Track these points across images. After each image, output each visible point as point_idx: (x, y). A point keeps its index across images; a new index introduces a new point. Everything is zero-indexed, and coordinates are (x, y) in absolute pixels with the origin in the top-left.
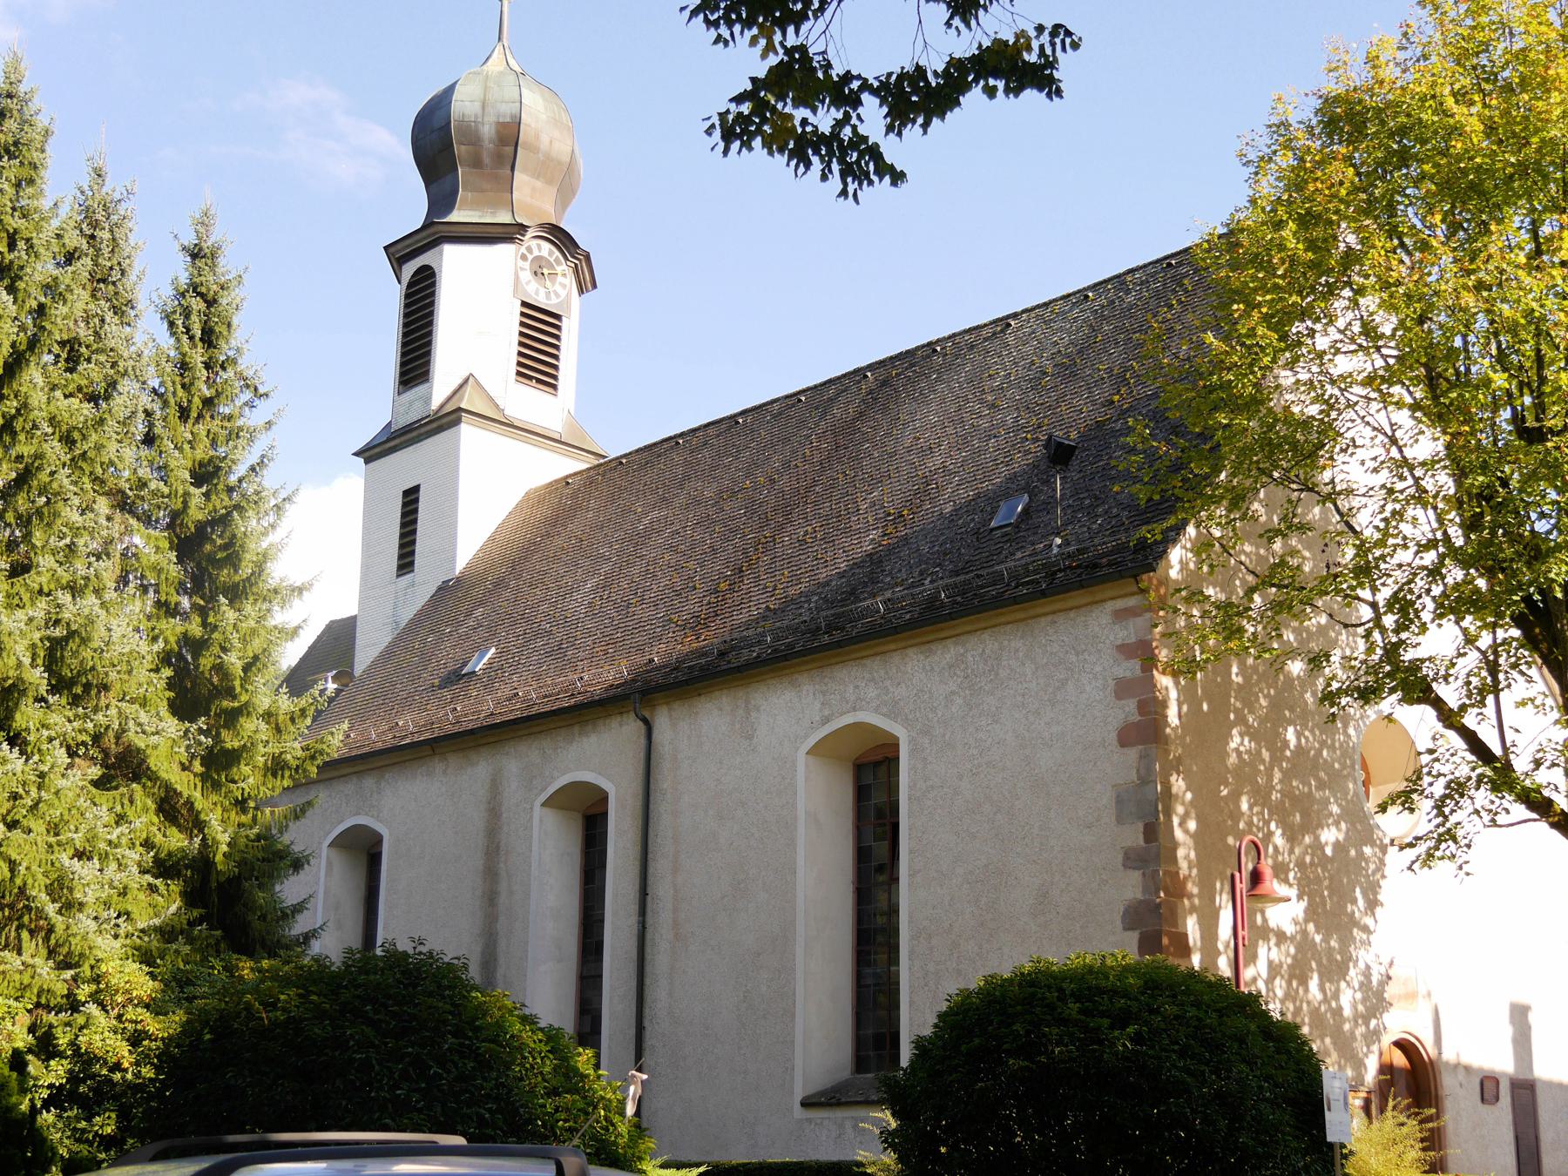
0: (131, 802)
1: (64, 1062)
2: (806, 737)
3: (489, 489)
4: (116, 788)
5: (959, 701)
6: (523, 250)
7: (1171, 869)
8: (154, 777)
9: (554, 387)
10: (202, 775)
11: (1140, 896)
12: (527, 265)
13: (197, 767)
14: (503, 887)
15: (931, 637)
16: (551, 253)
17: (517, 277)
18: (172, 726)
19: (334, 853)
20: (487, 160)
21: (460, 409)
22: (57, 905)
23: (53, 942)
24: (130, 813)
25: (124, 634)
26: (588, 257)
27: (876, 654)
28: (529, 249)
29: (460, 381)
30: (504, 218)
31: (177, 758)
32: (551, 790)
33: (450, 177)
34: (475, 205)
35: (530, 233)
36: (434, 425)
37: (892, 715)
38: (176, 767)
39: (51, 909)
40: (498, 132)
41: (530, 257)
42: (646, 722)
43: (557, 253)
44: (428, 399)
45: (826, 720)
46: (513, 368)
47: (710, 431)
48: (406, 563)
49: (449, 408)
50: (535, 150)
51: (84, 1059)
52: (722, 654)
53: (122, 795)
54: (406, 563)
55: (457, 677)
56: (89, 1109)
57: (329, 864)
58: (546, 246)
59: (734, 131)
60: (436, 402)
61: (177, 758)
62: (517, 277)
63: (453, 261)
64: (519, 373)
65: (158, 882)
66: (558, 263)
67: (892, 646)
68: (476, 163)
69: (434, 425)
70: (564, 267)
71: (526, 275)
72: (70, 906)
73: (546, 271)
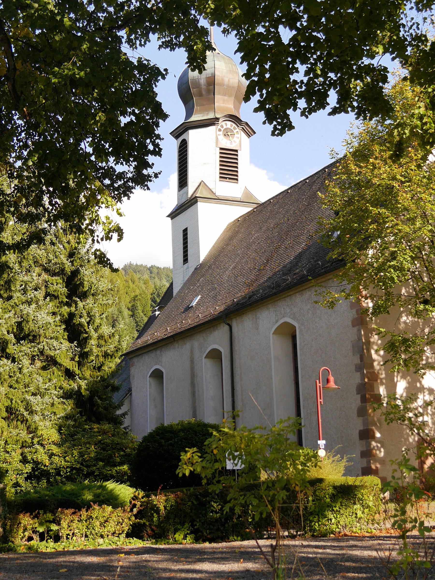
0: (53, 374)
1: (31, 465)
2: (272, 328)
3: (212, 225)
4: (49, 369)
5: (311, 312)
6: (219, 127)
7: (371, 371)
8: (60, 365)
9: (237, 180)
10: (78, 362)
11: (360, 382)
12: (221, 133)
13: (77, 359)
14: (196, 389)
15: (301, 289)
16: (231, 126)
17: (217, 139)
18: (66, 344)
19: (151, 379)
20: (204, 93)
21: (196, 197)
22: (28, 412)
23: (28, 425)
24: (53, 377)
25: (44, 317)
26: (247, 124)
27: (288, 296)
28: (222, 126)
29: (198, 184)
30: (211, 116)
31: (69, 356)
32: (207, 352)
33: (191, 102)
34: (201, 112)
35: (221, 120)
36: (190, 203)
37: (294, 319)
38: (68, 361)
39: (26, 413)
40: (207, 81)
41: (222, 129)
42: (229, 325)
43: (234, 125)
44: (187, 193)
45: (277, 321)
46: (218, 175)
47: (281, 196)
48: (186, 260)
49: (194, 196)
50: (222, 85)
51: (36, 463)
52: (250, 298)
53: (50, 372)
54: (186, 260)
55: (188, 308)
56: (39, 479)
57: (150, 384)
58: (229, 123)
59: (160, 155)
60: (190, 195)
61: (69, 356)
62: (217, 139)
63: (193, 136)
64: (221, 177)
65: (65, 400)
66: (235, 128)
67: (291, 293)
68: (200, 95)
69: (190, 203)
70: (238, 130)
71: (221, 137)
72: (32, 412)
73: (229, 134)
